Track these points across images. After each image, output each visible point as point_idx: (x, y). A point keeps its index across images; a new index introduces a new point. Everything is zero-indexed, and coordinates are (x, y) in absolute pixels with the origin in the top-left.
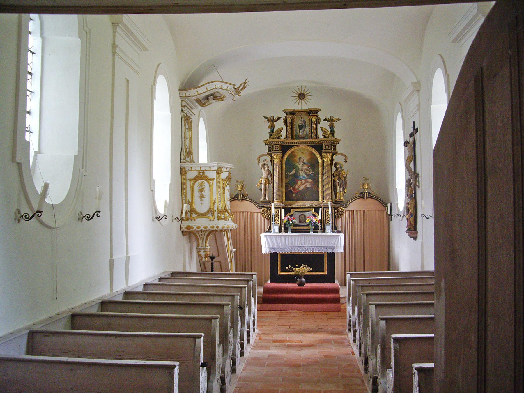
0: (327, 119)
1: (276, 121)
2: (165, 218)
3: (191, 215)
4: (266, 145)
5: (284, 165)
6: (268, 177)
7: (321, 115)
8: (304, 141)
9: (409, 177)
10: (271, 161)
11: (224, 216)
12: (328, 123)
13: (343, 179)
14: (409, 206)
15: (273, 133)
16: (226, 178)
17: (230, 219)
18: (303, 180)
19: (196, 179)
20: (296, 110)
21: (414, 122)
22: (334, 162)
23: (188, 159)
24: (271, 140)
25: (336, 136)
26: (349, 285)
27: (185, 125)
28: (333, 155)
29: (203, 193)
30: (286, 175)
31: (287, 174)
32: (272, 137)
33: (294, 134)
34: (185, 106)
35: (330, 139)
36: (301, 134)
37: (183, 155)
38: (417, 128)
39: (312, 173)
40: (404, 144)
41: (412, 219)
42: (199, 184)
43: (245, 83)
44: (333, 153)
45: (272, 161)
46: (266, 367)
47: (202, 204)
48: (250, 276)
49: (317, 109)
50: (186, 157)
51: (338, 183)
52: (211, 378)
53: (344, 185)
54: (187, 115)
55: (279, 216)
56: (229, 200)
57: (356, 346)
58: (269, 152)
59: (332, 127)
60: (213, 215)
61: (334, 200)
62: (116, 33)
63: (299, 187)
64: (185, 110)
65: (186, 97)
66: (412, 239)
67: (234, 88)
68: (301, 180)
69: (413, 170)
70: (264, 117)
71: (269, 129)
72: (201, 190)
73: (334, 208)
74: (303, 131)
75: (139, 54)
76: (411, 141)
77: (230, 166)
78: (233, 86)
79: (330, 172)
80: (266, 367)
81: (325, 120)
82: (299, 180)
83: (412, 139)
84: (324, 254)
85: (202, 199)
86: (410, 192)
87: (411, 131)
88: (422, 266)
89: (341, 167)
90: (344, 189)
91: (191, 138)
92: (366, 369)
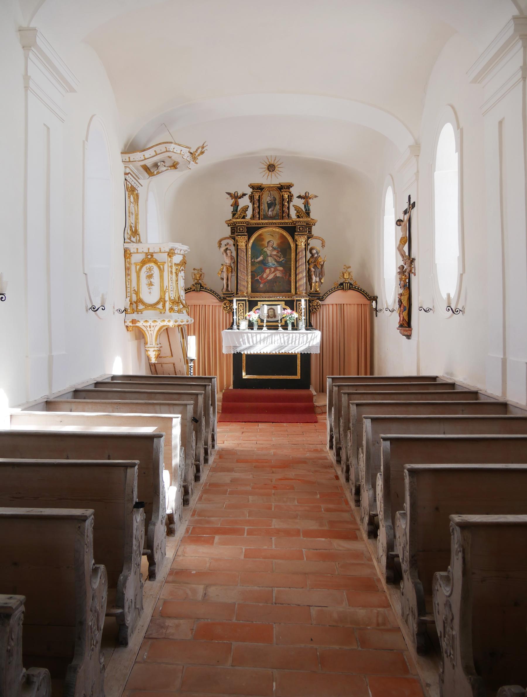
0: (302, 195)
1: (240, 198)
2: (102, 309)
3: (137, 307)
4: (228, 226)
5: (250, 250)
6: (231, 264)
7: (295, 191)
8: (274, 221)
9: (402, 263)
10: (234, 245)
11: (177, 307)
12: (303, 201)
13: (320, 267)
14: (402, 298)
15: (237, 212)
16: (180, 263)
17: (184, 311)
18: (272, 267)
19: (144, 263)
20: (264, 185)
21: (410, 196)
22: (309, 247)
23: (133, 239)
24: (235, 220)
25: (312, 215)
26: (331, 392)
27: (129, 197)
28: (308, 238)
29: (151, 280)
30: (252, 262)
31: (253, 260)
32: (236, 216)
33: (262, 213)
34: (129, 173)
35: (306, 219)
36: (270, 213)
37: (128, 233)
38: (414, 203)
39: (283, 260)
40: (397, 222)
41: (405, 313)
42: (147, 270)
43: (203, 148)
44: (308, 235)
45: (236, 245)
46: (227, 495)
47: (150, 293)
48: (209, 380)
49: (289, 183)
50: (131, 237)
51: (314, 271)
52: (153, 518)
53: (321, 275)
54: (132, 185)
55: (243, 309)
56: (183, 288)
57: (341, 469)
58: (232, 234)
59: (307, 205)
60: (164, 306)
61: (308, 292)
62: (29, 60)
63: (268, 276)
64: (129, 178)
65: (130, 161)
66: (404, 337)
67: (189, 152)
68: (270, 268)
69: (407, 254)
70: (227, 193)
71: (232, 207)
72: (150, 276)
73: (309, 302)
74: (273, 210)
75: (63, 96)
76: (405, 219)
77: (185, 248)
78: (188, 149)
79: (304, 259)
80: (227, 495)
81: (299, 197)
82: (266, 269)
83: (406, 217)
84: (297, 355)
85: (151, 287)
86: (404, 281)
87: (406, 206)
88: (418, 371)
89: (317, 253)
90: (320, 279)
91: (137, 215)
92: (358, 502)
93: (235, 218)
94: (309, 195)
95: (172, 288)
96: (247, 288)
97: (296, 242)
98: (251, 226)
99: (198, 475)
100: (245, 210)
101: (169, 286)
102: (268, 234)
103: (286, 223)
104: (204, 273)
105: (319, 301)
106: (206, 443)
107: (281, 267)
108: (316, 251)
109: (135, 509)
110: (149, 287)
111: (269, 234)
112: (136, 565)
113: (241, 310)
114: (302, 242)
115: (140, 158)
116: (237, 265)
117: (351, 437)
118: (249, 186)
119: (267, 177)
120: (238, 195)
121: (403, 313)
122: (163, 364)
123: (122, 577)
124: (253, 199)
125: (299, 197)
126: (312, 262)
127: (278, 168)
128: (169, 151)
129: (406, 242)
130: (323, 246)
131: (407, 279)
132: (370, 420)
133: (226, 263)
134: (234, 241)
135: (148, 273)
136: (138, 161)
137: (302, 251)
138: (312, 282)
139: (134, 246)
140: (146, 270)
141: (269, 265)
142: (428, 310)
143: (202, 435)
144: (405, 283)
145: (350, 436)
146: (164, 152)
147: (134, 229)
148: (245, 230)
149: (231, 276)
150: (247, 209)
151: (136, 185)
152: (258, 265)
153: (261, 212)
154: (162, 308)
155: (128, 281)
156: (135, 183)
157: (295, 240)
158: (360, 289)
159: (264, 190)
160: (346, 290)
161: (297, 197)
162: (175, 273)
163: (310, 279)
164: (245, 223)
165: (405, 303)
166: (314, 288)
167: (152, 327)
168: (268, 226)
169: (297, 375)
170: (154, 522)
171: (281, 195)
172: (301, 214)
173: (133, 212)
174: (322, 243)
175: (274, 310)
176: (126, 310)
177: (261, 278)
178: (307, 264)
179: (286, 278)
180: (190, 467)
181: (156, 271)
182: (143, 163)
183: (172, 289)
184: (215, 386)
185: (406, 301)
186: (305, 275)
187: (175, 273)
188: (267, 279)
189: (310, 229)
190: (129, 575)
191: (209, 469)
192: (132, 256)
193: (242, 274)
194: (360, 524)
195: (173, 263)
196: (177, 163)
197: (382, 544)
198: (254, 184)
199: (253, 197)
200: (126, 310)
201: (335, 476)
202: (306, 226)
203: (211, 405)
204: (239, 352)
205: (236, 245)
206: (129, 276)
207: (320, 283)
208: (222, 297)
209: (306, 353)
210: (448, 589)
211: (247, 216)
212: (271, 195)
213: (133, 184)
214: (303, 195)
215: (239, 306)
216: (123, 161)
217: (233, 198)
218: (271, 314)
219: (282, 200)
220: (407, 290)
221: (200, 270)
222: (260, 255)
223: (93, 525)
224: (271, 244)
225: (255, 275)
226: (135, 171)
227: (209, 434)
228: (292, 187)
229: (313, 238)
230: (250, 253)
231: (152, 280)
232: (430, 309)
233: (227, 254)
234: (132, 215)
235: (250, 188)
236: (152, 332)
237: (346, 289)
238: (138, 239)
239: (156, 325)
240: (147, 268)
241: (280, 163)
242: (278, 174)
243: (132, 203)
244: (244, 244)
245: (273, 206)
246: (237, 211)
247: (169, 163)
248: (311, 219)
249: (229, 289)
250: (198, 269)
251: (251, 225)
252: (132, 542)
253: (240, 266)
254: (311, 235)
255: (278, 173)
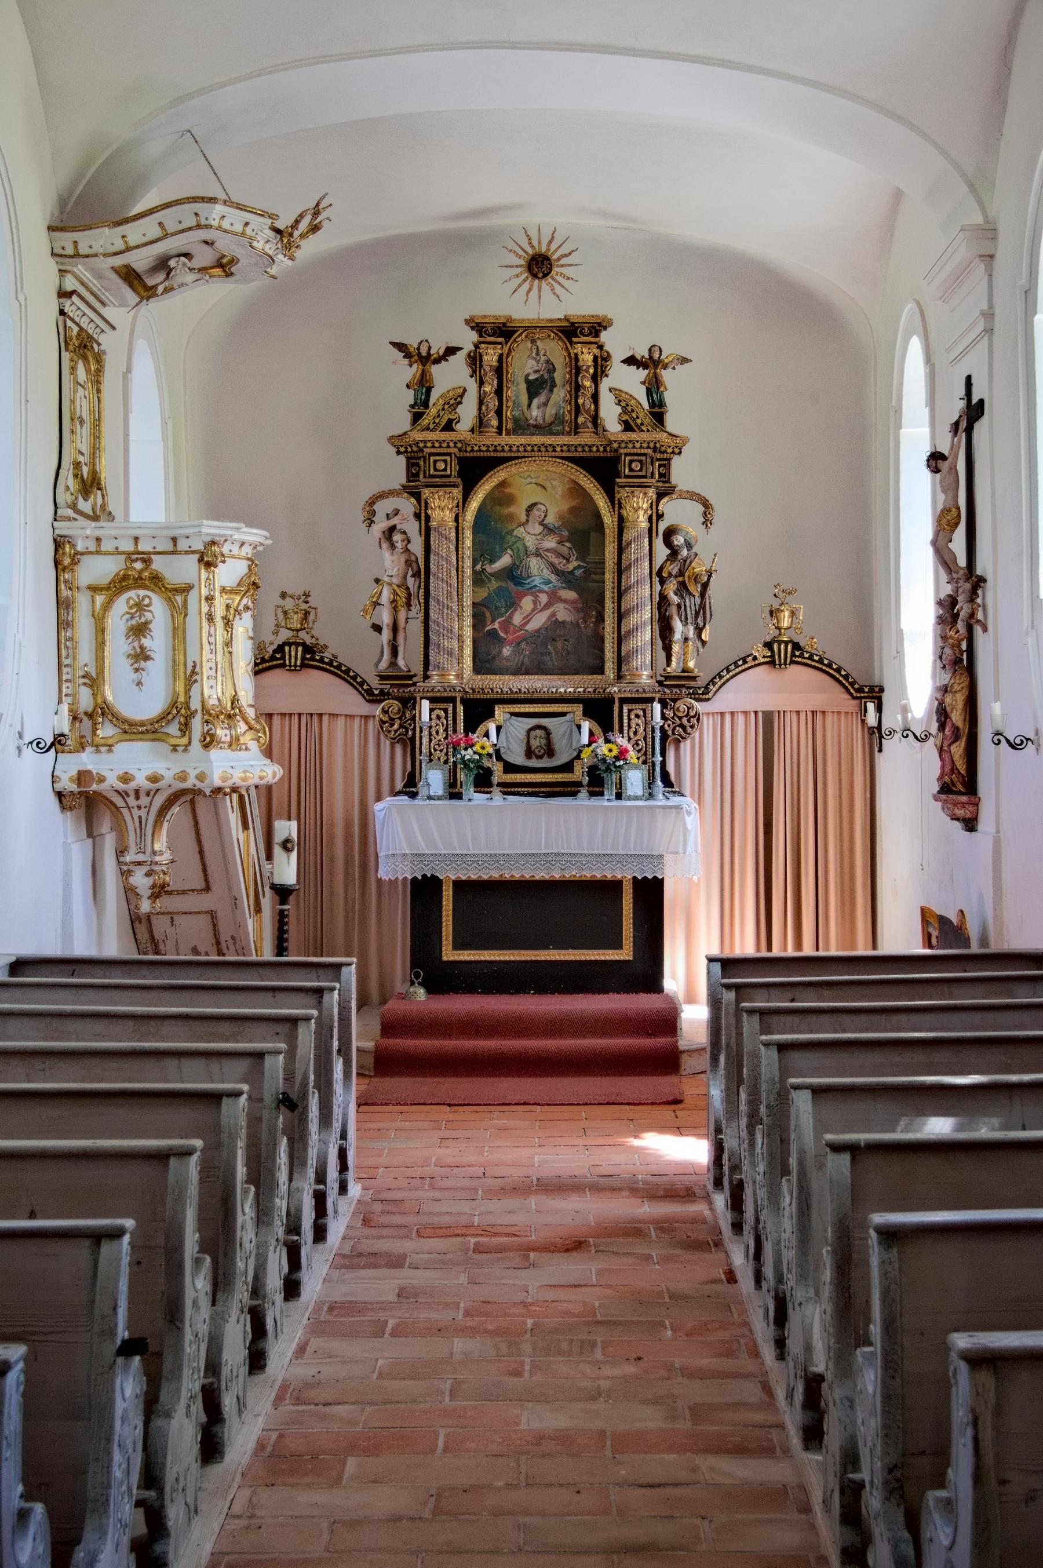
0: (639, 357)
1: (437, 361)
4: (399, 453)
5: (468, 534)
8: (549, 440)
10: (417, 516)
11: (227, 732)
12: (643, 374)
13: (695, 589)
14: (948, 699)
15: (427, 406)
16: (239, 585)
18: (541, 591)
19: (121, 584)
21: (969, 378)
22: (663, 526)
23: (85, 506)
24: (418, 436)
25: (673, 422)
28: (660, 496)
29: (143, 641)
30: (475, 572)
31: (478, 567)
32: (425, 421)
33: (508, 413)
34: (73, 292)
36: (535, 412)
37: (68, 488)
38: (981, 402)
39: (579, 567)
41: (958, 750)
42: (131, 608)
43: (316, 213)
44: (657, 487)
45: (422, 516)
47: (139, 683)
48: (330, 972)
50: (76, 498)
51: (679, 606)
54: (81, 329)
58: (409, 481)
59: (654, 388)
61: (660, 671)
63: (527, 619)
64: (74, 308)
65: (77, 255)
66: (957, 825)
68: (534, 591)
69: (962, 562)
70: (395, 344)
71: (412, 392)
72: (140, 630)
74: (545, 404)
77: (255, 535)
79: (647, 564)
81: (631, 361)
82: (523, 595)
85: (143, 664)
86: (953, 647)
89: (689, 546)
90: (699, 630)
91: (97, 423)
93: (419, 428)
94: (661, 354)
95: (211, 669)
96: (460, 660)
97: (620, 507)
98: (472, 454)
99: (294, 1277)
100: (452, 402)
101: (201, 662)
102: (529, 480)
103: (586, 445)
104: (315, 609)
105: (693, 701)
106: (321, 1177)
107: (570, 588)
108: (685, 540)
109: (120, 1360)
110: (136, 666)
111: (533, 481)
112: (119, 1526)
113: (437, 733)
114: (639, 508)
115: (112, 244)
116: (425, 578)
117: (765, 1146)
118: (467, 322)
119: (527, 295)
120: (432, 352)
121: (952, 748)
122: (175, 917)
123: (82, 1554)
124: (481, 366)
125: (631, 361)
126: (670, 575)
127: (562, 266)
128: (208, 227)
129: (957, 524)
130: (707, 522)
131: (962, 640)
132: (807, 1095)
133: (392, 576)
134: (415, 503)
135: (132, 618)
136: (105, 255)
137: (637, 538)
138: (670, 641)
139: (88, 532)
140: (127, 609)
141: (534, 584)
142: (1019, 742)
143: (310, 1149)
144: (957, 652)
145: (763, 1144)
146: (190, 229)
147: (85, 470)
148: (454, 468)
149: (407, 619)
150: (459, 399)
151: (87, 320)
152: (494, 584)
153: (504, 408)
154: (179, 734)
155: (65, 645)
156: (92, 321)
157: (617, 502)
158: (826, 662)
159: (515, 336)
160: (783, 666)
161: (624, 361)
162: (222, 617)
163: (665, 630)
164: (452, 444)
165: (957, 717)
166: (678, 659)
167: (142, 794)
168: (530, 454)
169: (621, 948)
170: (167, 1408)
171: (573, 356)
172: (638, 417)
173: (84, 417)
174: (705, 513)
175: (548, 732)
176: (60, 740)
177: (507, 625)
178: (656, 579)
179: (586, 627)
180: (272, 1248)
181: (158, 610)
182: (119, 261)
183: (212, 673)
184: (350, 991)
185: (959, 712)
186: (648, 615)
187: (222, 617)
188: (526, 631)
189: (664, 466)
190: (102, 1547)
191: (331, 1259)
192: (81, 561)
193: (443, 613)
194: (786, 1409)
195: (217, 588)
196: (233, 261)
197: (834, 1456)
198: (485, 317)
199: (481, 361)
200: (60, 740)
201: (724, 1273)
202: (652, 458)
203: (339, 1051)
204: (429, 875)
205: (423, 518)
206: (70, 630)
207: (699, 644)
208: (376, 689)
209: (650, 877)
210: (949, 1531)
211: (458, 422)
212: (538, 354)
213: (87, 322)
214: (643, 357)
215: (434, 716)
216: (55, 252)
217: (413, 360)
218: (539, 744)
219: (574, 371)
220: (962, 674)
221: (303, 598)
222: (503, 551)
223: (22, 1388)
224: (537, 513)
225: (484, 615)
226: (94, 284)
227: (331, 1145)
228: (609, 329)
229: (674, 496)
230: (468, 543)
231: (146, 642)
232: (1027, 740)
233: (393, 546)
234: (82, 426)
235: (469, 329)
236: (143, 813)
237: (782, 661)
238: (100, 501)
239: (157, 790)
240: (131, 602)
241: (567, 252)
242: (563, 286)
243: (81, 385)
244: (448, 516)
245: (544, 389)
246: (426, 404)
247: (204, 257)
248: (670, 434)
249: (401, 662)
250: (297, 594)
251: (472, 451)
252: (109, 1453)
253: (436, 588)
254: (667, 485)
255: (560, 284)
